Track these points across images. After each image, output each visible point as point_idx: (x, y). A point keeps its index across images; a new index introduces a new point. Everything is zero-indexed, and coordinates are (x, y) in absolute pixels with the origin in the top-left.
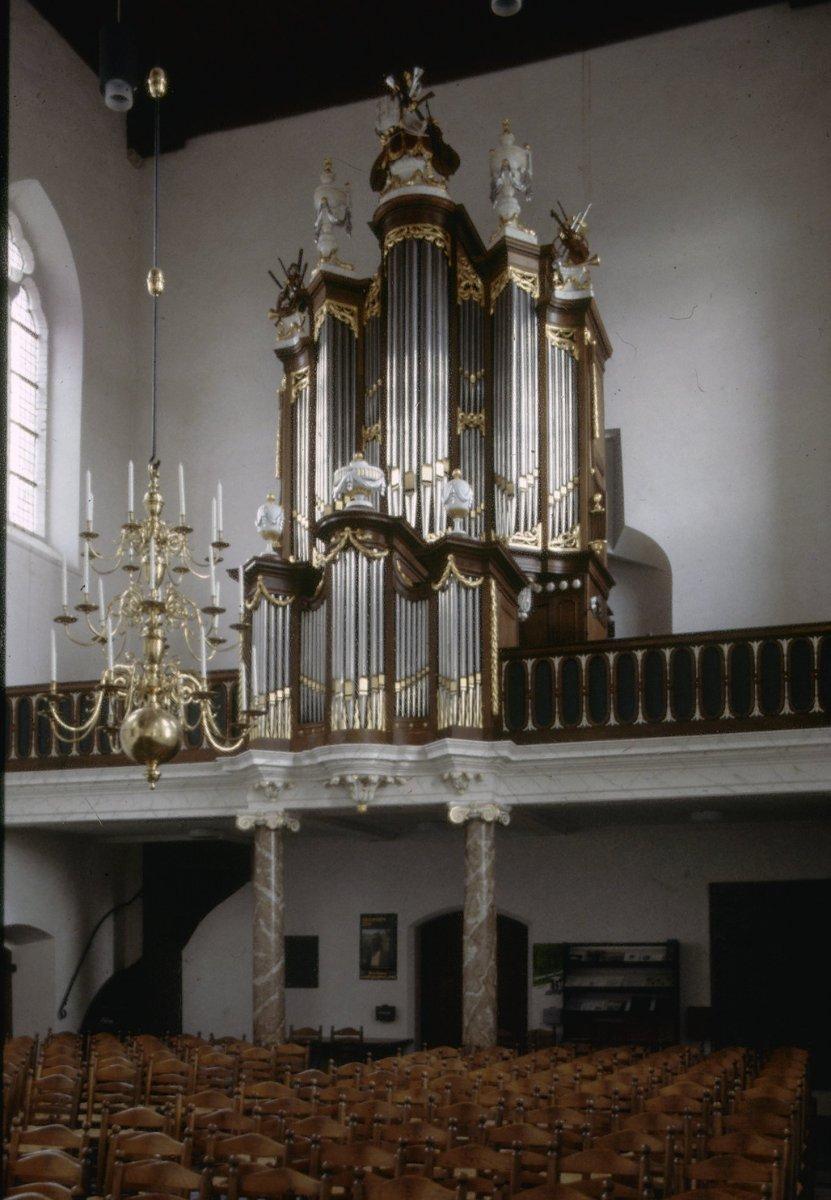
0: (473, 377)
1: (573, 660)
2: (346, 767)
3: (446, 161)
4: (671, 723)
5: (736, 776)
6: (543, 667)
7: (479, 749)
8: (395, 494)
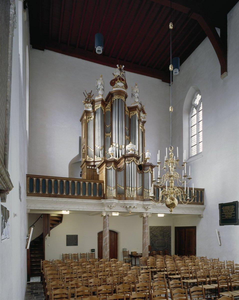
0: (108, 126)
1: (95, 183)
2: (132, 205)
3: (126, 87)
4: (53, 195)
5: (185, 211)
6: (90, 183)
7: (116, 201)
8: (123, 150)
